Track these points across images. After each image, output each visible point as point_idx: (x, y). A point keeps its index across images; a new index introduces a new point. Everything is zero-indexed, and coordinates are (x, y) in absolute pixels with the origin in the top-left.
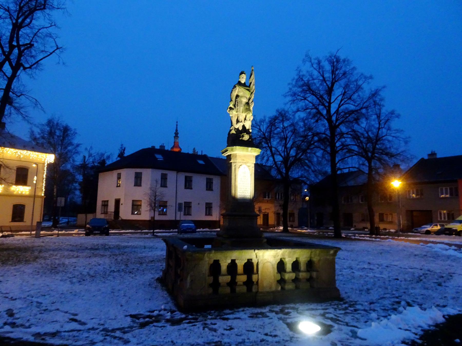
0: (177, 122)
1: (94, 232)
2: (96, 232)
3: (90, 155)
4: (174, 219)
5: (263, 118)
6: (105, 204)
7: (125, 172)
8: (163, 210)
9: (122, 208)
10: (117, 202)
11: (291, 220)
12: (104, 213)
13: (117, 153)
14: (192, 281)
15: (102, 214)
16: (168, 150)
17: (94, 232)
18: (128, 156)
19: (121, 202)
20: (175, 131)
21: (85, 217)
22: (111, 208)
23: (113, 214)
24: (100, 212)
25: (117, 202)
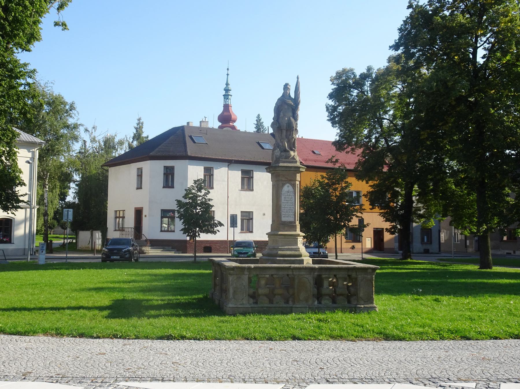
0: (228, 69)
1: (112, 257)
2: (115, 257)
3: (93, 140)
4: (233, 239)
5: (365, 71)
6: (120, 216)
7: (147, 166)
8: (344, 144)
9: (145, 222)
10: (139, 213)
11: (426, 240)
12: (119, 230)
13: (132, 132)
14: (234, 292)
15: (115, 230)
16: (213, 129)
17: (112, 257)
18: (151, 140)
19: (145, 212)
20: (221, 110)
21: (90, 236)
22: (130, 222)
23: (133, 230)
24: (113, 229)
25: (139, 213)
